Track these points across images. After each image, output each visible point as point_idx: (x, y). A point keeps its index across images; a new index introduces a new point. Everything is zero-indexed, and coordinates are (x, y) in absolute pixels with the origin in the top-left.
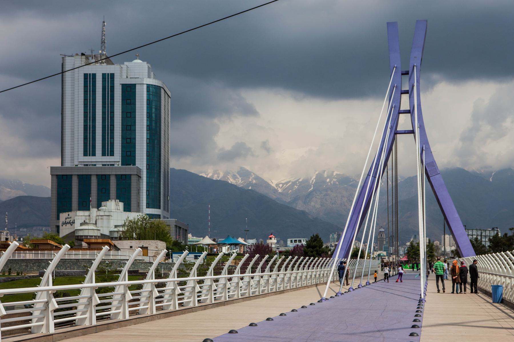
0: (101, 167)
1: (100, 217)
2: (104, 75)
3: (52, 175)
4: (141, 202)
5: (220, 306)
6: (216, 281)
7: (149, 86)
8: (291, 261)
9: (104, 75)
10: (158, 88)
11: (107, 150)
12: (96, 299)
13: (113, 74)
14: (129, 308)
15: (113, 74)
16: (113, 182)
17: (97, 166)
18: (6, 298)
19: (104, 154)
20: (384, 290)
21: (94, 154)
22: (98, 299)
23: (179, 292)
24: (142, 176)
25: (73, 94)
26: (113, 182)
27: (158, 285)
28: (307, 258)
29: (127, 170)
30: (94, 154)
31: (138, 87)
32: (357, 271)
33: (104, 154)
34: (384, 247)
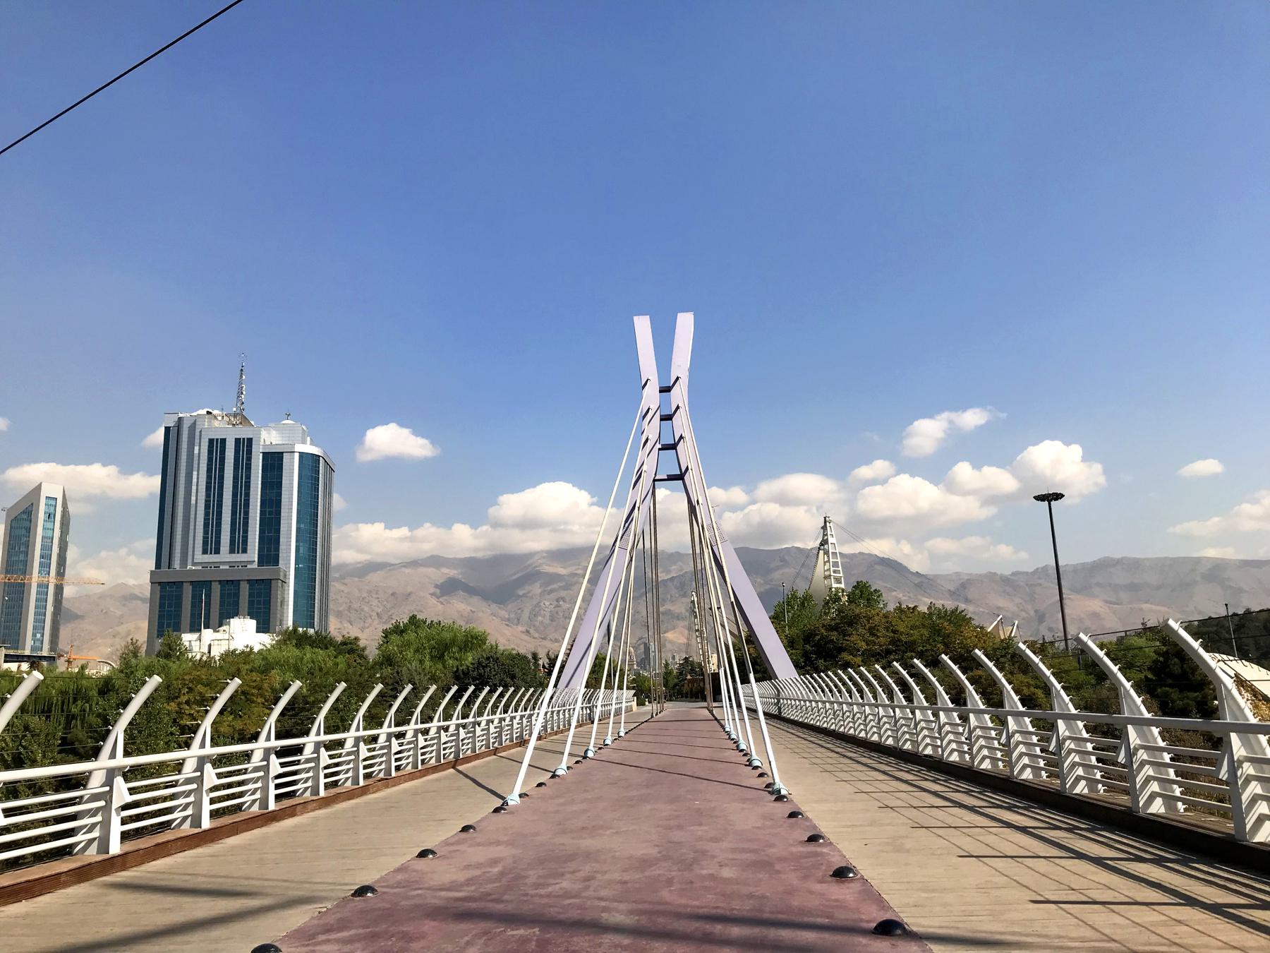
0: (227, 569)
1: (216, 642)
2: (237, 441)
3: (152, 583)
4: (285, 619)
5: (1230, 560)
6: (401, 735)
7: (302, 455)
8: (501, 695)
9: (237, 441)
10: (316, 458)
11: (239, 544)
12: (275, 765)
13: (252, 439)
14: (395, 762)
15: (252, 439)
16: (245, 589)
17: (221, 568)
18: (12, 790)
19: (232, 551)
20: (659, 739)
21: (217, 551)
22: (328, 758)
23: (365, 754)
24: (287, 581)
25: (727, 682)
26: (245, 589)
27: (329, 746)
28: (532, 689)
29: (266, 572)
30: (217, 551)
31: (286, 457)
32: (581, 713)
33: (232, 551)
34: (211, 545)
